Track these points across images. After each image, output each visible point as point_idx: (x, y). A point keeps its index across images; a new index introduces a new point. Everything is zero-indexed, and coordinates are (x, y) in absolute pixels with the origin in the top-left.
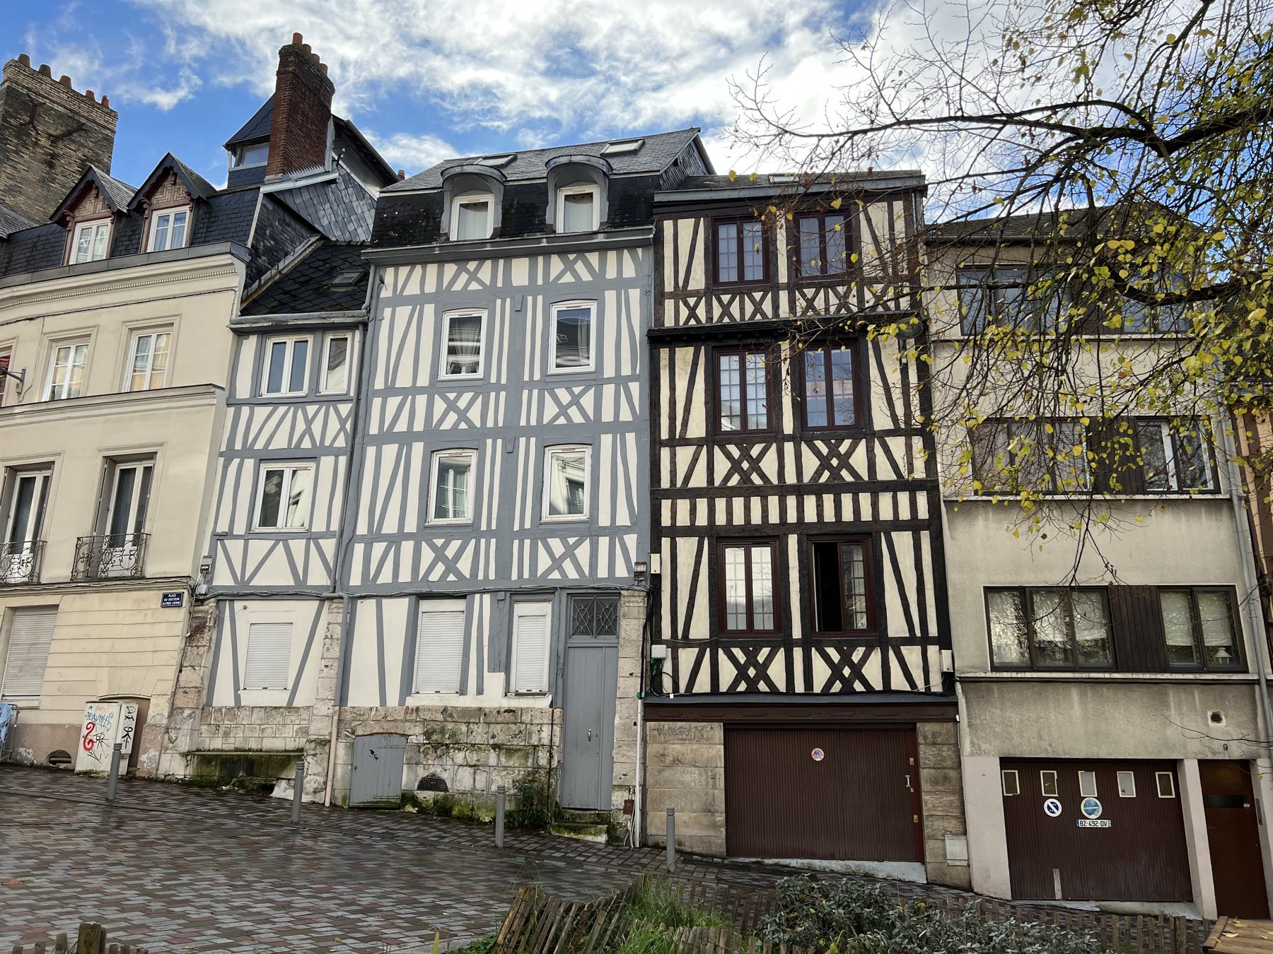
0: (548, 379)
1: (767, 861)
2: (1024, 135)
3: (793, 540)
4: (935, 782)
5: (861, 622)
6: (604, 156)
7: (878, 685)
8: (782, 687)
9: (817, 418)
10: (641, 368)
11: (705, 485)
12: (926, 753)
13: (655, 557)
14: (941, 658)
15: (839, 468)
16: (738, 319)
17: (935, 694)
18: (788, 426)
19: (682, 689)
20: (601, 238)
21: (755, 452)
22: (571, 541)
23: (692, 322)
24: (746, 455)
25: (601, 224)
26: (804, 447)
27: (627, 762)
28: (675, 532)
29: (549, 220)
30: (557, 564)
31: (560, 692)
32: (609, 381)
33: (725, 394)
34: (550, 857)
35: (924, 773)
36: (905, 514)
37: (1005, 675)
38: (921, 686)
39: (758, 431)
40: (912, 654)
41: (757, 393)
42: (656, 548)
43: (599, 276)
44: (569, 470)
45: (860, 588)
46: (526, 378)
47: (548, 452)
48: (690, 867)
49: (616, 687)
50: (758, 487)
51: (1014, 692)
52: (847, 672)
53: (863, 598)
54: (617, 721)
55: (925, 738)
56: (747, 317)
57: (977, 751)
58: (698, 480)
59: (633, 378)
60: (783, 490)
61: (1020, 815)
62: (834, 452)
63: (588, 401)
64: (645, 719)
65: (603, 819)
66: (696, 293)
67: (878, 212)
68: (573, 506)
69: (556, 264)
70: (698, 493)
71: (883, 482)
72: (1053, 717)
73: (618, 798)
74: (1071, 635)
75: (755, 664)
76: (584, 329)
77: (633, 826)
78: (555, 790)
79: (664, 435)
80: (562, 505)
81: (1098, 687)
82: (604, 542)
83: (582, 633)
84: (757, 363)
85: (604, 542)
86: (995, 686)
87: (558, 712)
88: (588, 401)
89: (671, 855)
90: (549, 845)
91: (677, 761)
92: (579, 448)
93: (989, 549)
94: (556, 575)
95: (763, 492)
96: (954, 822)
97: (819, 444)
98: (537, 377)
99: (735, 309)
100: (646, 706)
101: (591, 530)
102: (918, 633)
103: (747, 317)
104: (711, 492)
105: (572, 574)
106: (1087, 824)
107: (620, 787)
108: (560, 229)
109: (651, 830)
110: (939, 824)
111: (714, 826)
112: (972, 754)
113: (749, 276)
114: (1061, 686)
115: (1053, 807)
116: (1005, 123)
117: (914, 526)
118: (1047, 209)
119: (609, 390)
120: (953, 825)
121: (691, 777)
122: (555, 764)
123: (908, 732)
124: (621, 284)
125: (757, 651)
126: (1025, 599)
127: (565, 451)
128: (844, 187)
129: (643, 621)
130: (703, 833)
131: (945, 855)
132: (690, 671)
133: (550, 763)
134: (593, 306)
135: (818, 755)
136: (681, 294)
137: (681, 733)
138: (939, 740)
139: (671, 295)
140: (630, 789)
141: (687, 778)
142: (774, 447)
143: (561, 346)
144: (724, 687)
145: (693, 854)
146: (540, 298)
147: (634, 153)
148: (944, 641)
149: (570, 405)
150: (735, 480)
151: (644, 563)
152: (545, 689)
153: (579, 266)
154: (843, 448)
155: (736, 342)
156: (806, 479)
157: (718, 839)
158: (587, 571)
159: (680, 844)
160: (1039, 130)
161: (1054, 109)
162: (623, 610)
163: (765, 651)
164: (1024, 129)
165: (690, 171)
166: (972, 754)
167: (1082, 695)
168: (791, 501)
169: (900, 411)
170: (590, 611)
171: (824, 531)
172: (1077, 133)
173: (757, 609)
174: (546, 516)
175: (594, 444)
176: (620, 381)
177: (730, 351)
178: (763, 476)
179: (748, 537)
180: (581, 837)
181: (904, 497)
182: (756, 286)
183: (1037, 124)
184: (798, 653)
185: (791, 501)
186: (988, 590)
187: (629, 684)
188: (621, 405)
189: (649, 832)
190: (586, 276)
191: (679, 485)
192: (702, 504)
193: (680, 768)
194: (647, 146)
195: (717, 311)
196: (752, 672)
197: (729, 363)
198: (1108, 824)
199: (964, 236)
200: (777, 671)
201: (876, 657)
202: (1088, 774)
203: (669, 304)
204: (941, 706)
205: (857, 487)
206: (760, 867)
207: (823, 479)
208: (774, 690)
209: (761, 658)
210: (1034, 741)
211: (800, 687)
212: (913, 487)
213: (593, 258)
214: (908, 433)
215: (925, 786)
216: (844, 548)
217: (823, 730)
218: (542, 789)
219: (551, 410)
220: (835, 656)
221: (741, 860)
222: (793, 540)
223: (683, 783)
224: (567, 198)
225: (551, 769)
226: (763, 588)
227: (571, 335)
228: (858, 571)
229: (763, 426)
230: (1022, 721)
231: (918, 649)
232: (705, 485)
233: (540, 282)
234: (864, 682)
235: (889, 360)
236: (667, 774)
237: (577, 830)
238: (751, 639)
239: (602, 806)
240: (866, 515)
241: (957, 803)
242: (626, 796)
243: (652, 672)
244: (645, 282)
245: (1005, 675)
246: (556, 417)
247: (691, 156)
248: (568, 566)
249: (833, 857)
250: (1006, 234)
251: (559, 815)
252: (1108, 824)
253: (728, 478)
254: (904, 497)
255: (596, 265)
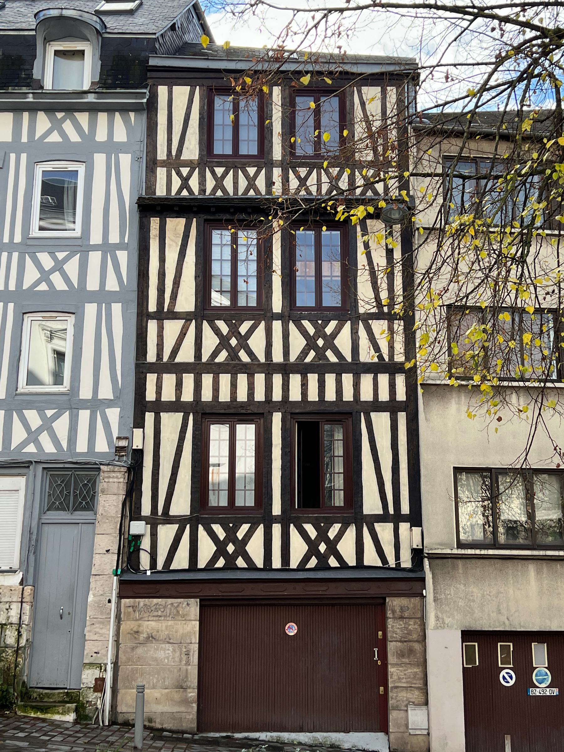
0: (30, 242)
1: (238, 735)
2: (493, 29)
3: (277, 418)
4: (401, 654)
5: (339, 500)
6: (98, 13)
7: (351, 561)
8: (260, 563)
9: (305, 298)
10: (131, 236)
11: (192, 360)
12: (394, 627)
13: (138, 432)
14: (411, 536)
15: (325, 348)
16: (231, 194)
17: (404, 569)
18: (277, 305)
19: (160, 567)
20: (91, 98)
21: (244, 328)
22: (49, 413)
23: (185, 193)
24: (234, 331)
25: (92, 83)
26: (292, 326)
27: (99, 641)
28: (159, 407)
29: (36, 75)
30: (33, 436)
31: (31, 570)
32: (96, 248)
33: (216, 269)
34: (13, 738)
35: (392, 647)
36: (384, 396)
37: (470, 552)
38: (392, 563)
39: (247, 308)
40: (385, 531)
41: (249, 268)
42: (139, 423)
43: (88, 138)
44: (55, 341)
45: (339, 467)
46: (6, 240)
47: (27, 319)
48: (159, 744)
49: (90, 565)
50: (245, 365)
51: (477, 568)
52: (322, 548)
53: (342, 476)
54: (91, 598)
55: (394, 612)
56: (241, 191)
57: (441, 625)
58: (186, 355)
59: (121, 246)
60: (269, 368)
61: (477, 684)
62: (320, 332)
63: (72, 267)
64: (121, 596)
65: (72, 698)
66: (186, 164)
67: (371, 93)
68: (58, 378)
69: (43, 121)
70: (184, 368)
71: (365, 364)
72: (511, 591)
73: (89, 677)
74: (531, 516)
75: (235, 541)
76: (71, 193)
77: (103, 704)
78: (22, 671)
79: (152, 307)
80: (46, 376)
81: (553, 564)
82: (84, 415)
83: (57, 509)
84: (248, 239)
85: (84, 415)
86: (460, 563)
87: (28, 589)
88: (72, 267)
89: (138, 730)
90: (12, 726)
91: (151, 638)
92: (61, 316)
93: (457, 432)
94: (31, 448)
95: (249, 370)
96: (417, 693)
97: (306, 324)
98: (18, 239)
99: (228, 183)
100: (122, 583)
101: (71, 403)
102: (391, 511)
103: (241, 191)
104: (198, 368)
105: (49, 448)
106: (537, 692)
107: (91, 665)
108: (48, 85)
109: (122, 708)
110: (403, 695)
111: (186, 702)
112: (436, 628)
113: (243, 150)
114: (520, 563)
115: (507, 677)
116: (476, 16)
117: (392, 407)
118: (513, 106)
119: (95, 258)
120: (416, 695)
121: (165, 653)
122: (23, 642)
123: (379, 605)
124: (111, 148)
125: (237, 528)
126: (491, 478)
127: (45, 319)
128: (332, 68)
129: (122, 498)
130: (175, 709)
131: (407, 726)
132: (166, 548)
133: (18, 641)
134: (81, 169)
135: (292, 630)
136: (174, 163)
137: (157, 610)
138: (406, 614)
139: (164, 164)
140: (101, 667)
141: (161, 654)
142: (263, 324)
143: (44, 207)
144: (202, 563)
145: (163, 730)
146: (24, 156)
147: (130, 13)
148: (415, 518)
149: (52, 271)
150: (222, 357)
151: (126, 438)
152: (16, 566)
153: (68, 126)
154: (329, 330)
155: (228, 217)
156: (293, 358)
157: (189, 716)
158: (65, 445)
159: (150, 720)
160: (509, 27)
161: (524, 6)
162: (102, 485)
163: (245, 528)
164: (496, 22)
165: (189, 38)
166: (436, 628)
167: (539, 572)
168: (277, 379)
169: (384, 295)
170: (67, 486)
171: (307, 410)
172: (544, 32)
173: (239, 485)
174: (23, 386)
175: (77, 313)
176: (107, 248)
177: (221, 225)
178: (250, 353)
179: (233, 414)
180: (48, 716)
181: (383, 379)
182: (250, 160)
183: (506, 20)
184: (277, 529)
185: (277, 379)
186: (458, 470)
187: (105, 561)
188: (111, 274)
189: (119, 709)
190: (74, 137)
191: (165, 359)
192: (189, 380)
193: (154, 645)
194: (145, 7)
195: (210, 183)
196: (322, 548)
197: (220, 239)
198: (556, 691)
199: (442, 127)
200: (255, 548)
201: (351, 532)
202: (541, 645)
203: (161, 173)
204: (410, 581)
205: (340, 369)
206: (229, 742)
207: (308, 359)
208: (252, 567)
209: (240, 535)
210: (494, 615)
211: (277, 563)
212: (392, 369)
213: (83, 118)
214: (391, 318)
215: (391, 659)
216: (327, 427)
217: (248, 605)
218: (9, 669)
219: (31, 275)
220: (312, 532)
221: (212, 735)
222: (277, 418)
223: (156, 660)
224: (57, 53)
225: (18, 648)
226: (246, 465)
227: (57, 196)
228: (339, 450)
229: (253, 303)
230: (483, 596)
231: (390, 526)
232: (192, 360)
233: (24, 139)
234: (339, 558)
235: (376, 244)
236: (140, 651)
237: (45, 709)
238: (232, 515)
239: (72, 685)
240: (348, 396)
241: (420, 675)
242: (97, 673)
243: (130, 548)
244: (137, 148)
245: (470, 552)
246: (38, 283)
247: (189, 22)
248: (44, 438)
249: (301, 730)
250: (503, 130)
251: (26, 694)
252: (556, 691)
253: (215, 353)
254: (383, 379)
255: (85, 126)
